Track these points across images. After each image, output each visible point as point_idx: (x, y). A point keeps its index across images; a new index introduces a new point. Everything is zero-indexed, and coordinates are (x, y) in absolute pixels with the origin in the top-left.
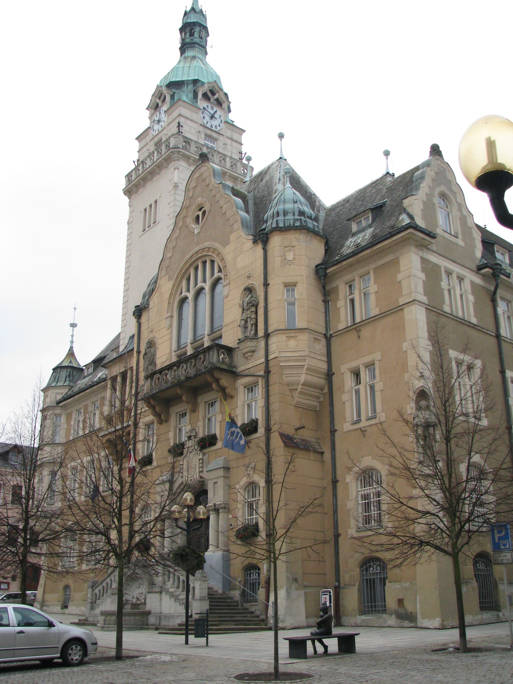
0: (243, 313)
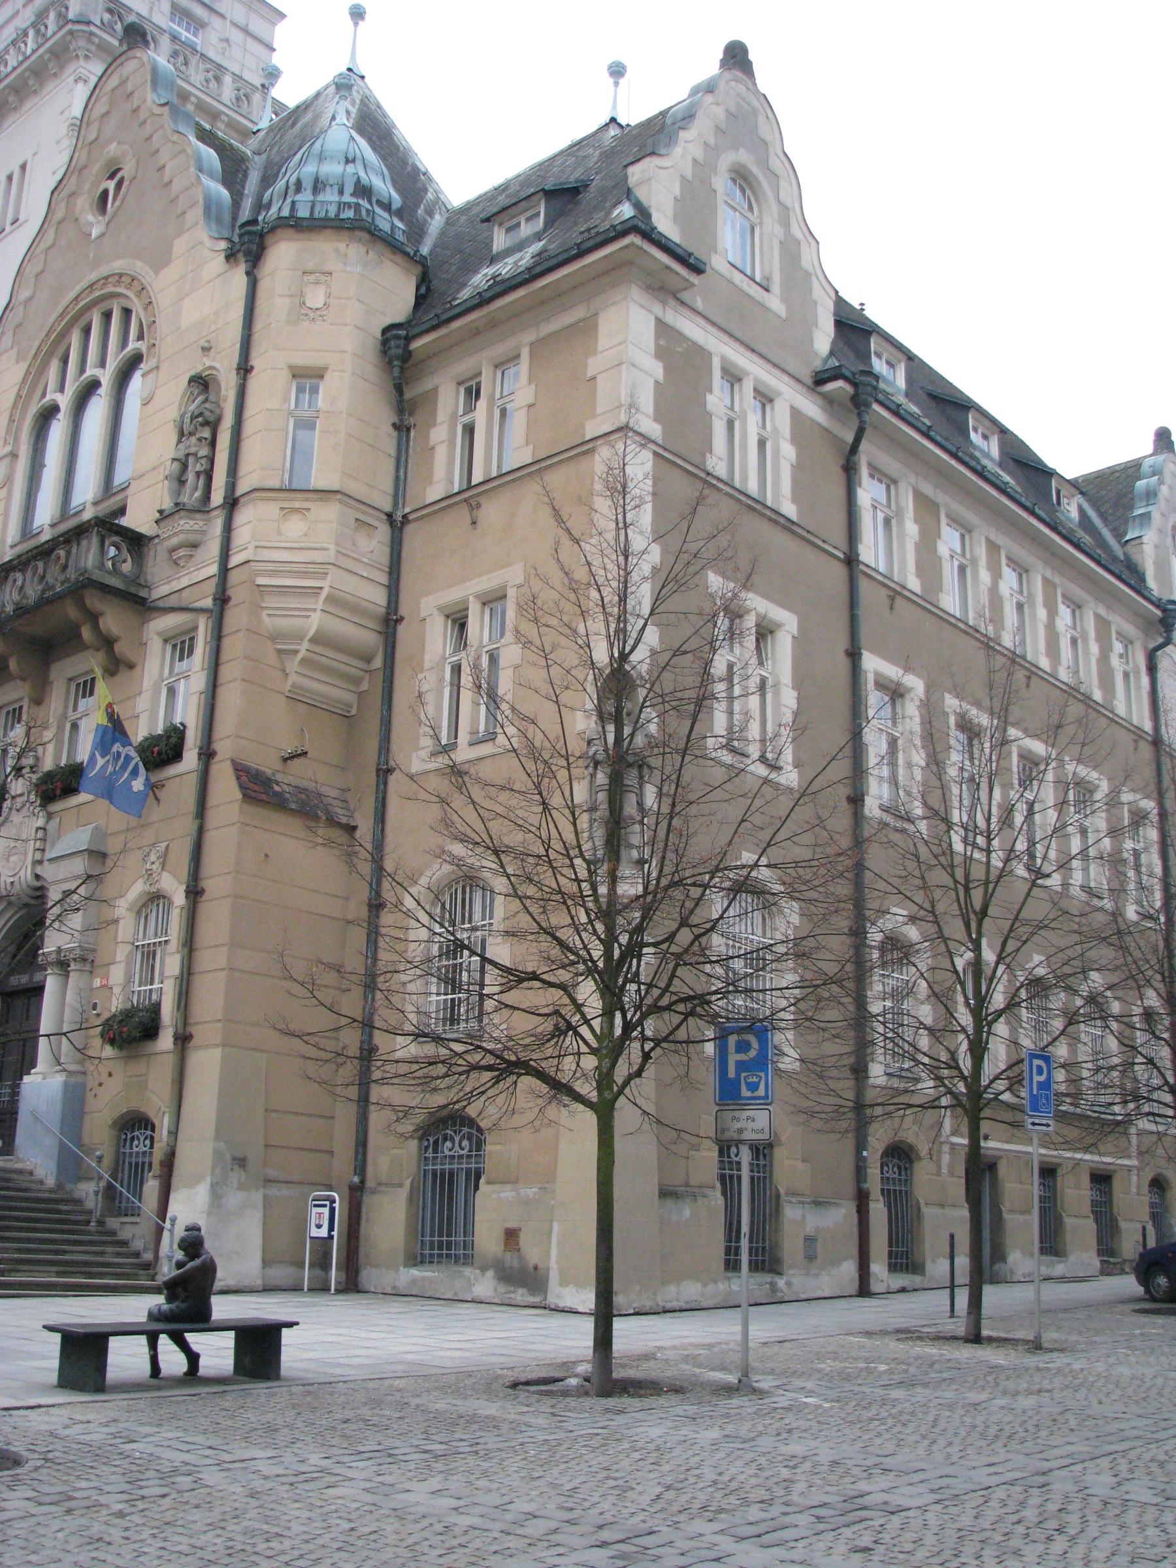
0: (179, 442)
